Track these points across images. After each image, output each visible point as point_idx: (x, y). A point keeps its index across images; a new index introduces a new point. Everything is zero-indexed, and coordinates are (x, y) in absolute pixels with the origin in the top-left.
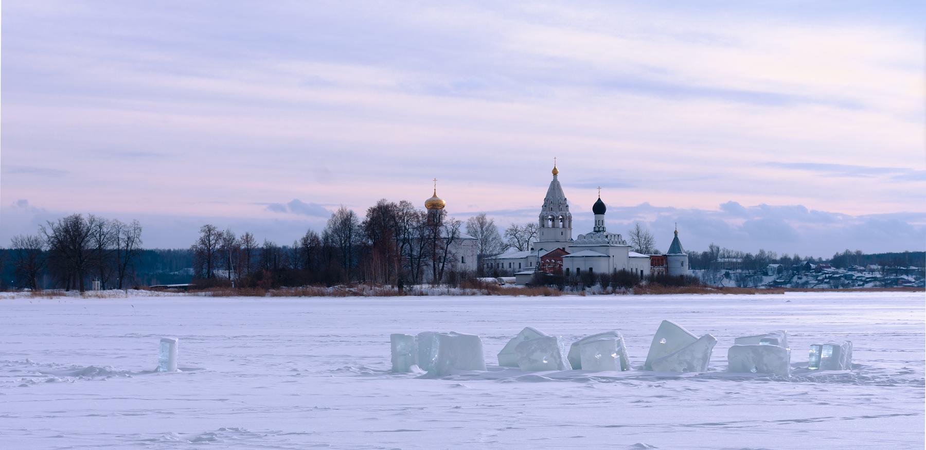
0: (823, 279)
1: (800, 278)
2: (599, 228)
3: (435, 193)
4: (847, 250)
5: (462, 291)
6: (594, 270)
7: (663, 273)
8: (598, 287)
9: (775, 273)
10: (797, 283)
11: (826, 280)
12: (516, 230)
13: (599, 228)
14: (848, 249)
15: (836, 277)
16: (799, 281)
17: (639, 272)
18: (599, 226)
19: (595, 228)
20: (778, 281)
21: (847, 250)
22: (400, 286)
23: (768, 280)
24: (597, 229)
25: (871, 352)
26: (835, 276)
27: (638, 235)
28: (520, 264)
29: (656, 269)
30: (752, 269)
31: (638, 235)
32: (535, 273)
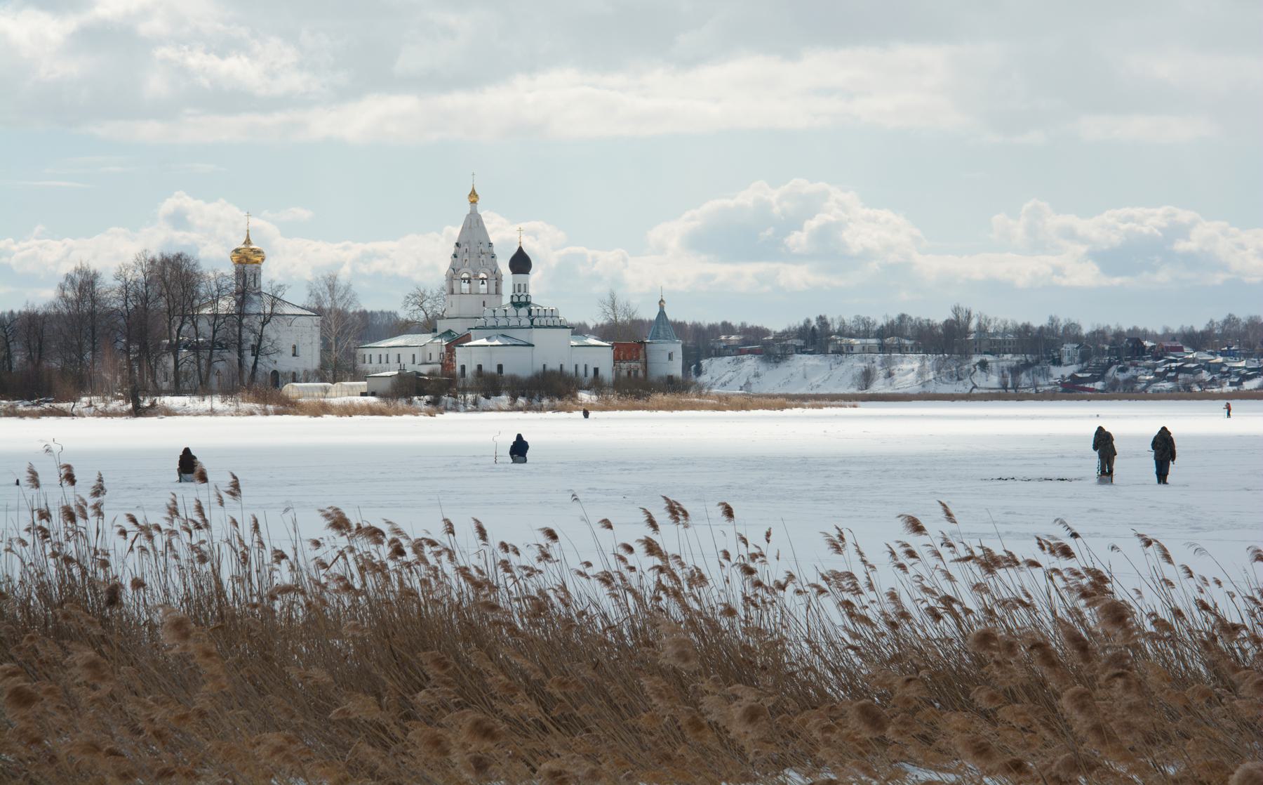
0: (1166, 372)
1: (1123, 370)
2: (519, 297)
3: (248, 236)
4: (1230, 315)
5: (233, 408)
6: (484, 368)
7: (636, 372)
8: (504, 399)
9: (1077, 359)
10: (1116, 381)
11: (1169, 374)
12: (423, 295)
13: (519, 297)
14: (1232, 312)
15: (1190, 368)
16: (1121, 377)
17: (591, 373)
18: (519, 294)
19: (512, 296)
20: (1080, 375)
21: (1230, 315)
22: (133, 396)
23: (1059, 373)
24: (516, 300)
25: (952, 510)
26: (1188, 366)
27: (613, 307)
28: (414, 355)
29: (625, 365)
30: (1031, 353)
31: (613, 307)
32: (399, 374)
